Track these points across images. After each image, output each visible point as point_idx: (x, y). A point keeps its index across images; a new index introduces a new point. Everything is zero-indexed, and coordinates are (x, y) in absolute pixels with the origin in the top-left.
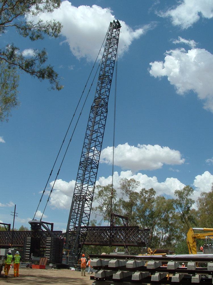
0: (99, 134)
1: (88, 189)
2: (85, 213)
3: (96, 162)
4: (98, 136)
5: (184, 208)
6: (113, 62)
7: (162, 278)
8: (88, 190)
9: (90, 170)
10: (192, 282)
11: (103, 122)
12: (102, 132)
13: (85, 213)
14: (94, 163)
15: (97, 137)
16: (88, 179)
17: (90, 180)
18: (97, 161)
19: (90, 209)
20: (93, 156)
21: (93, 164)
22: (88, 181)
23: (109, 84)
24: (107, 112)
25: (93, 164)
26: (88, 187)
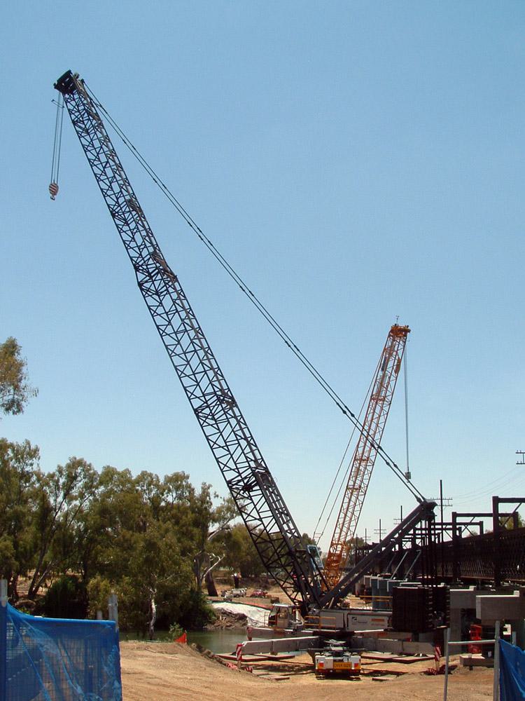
0: (169, 330)
1: (228, 451)
2: (231, 469)
3: (205, 421)
4: (176, 345)
5: (237, 587)
6: (128, 243)
7: (519, 504)
8: (226, 448)
9: (207, 398)
10: (500, 512)
11: (159, 321)
12: (166, 338)
13: (231, 469)
14: (209, 417)
15: (179, 343)
16: (199, 377)
17: (193, 377)
18: (205, 424)
19: (251, 534)
20: (197, 381)
21: (209, 415)
22: (228, 444)
23: (135, 259)
24: (140, 285)
25: (209, 415)
26: (230, 453)
